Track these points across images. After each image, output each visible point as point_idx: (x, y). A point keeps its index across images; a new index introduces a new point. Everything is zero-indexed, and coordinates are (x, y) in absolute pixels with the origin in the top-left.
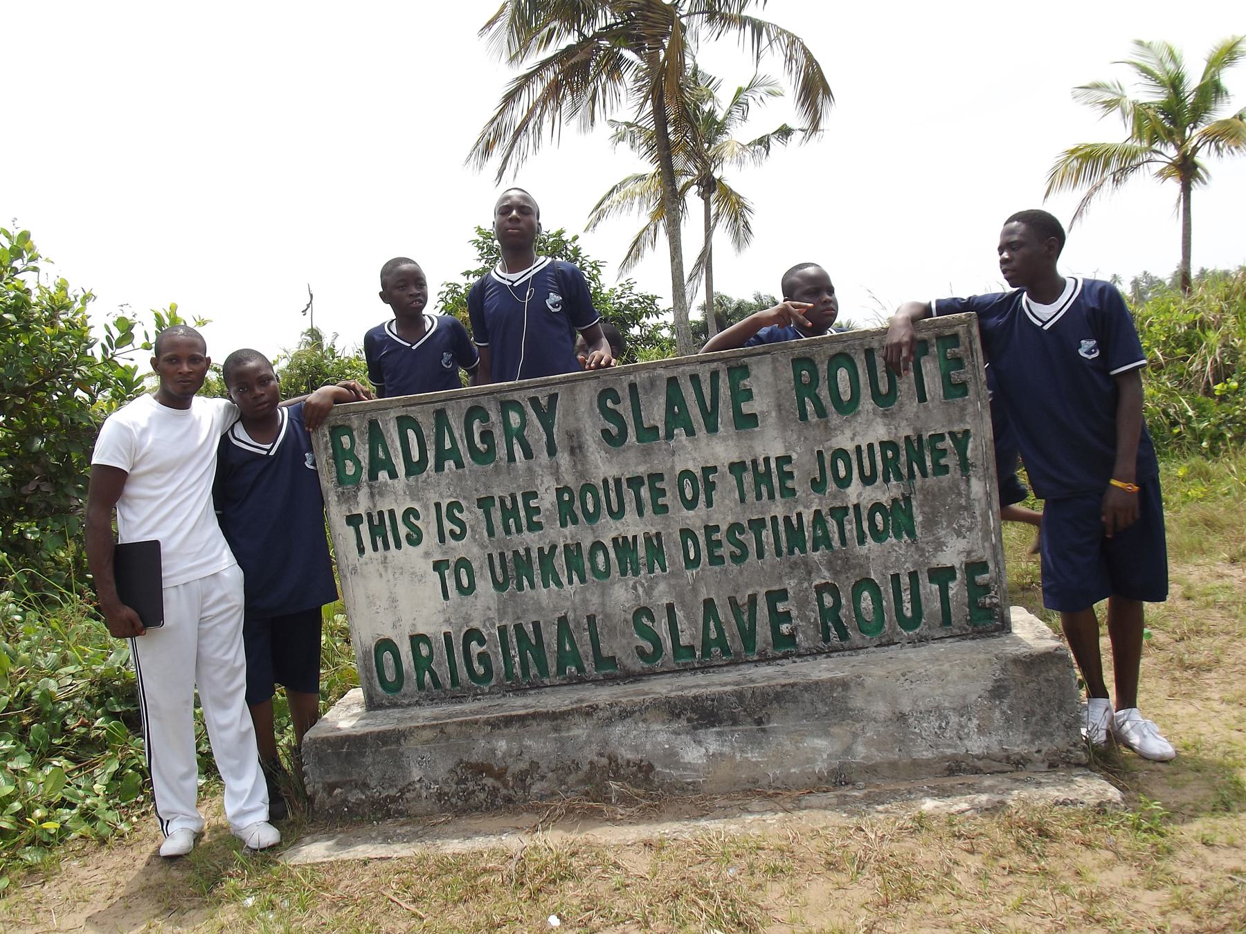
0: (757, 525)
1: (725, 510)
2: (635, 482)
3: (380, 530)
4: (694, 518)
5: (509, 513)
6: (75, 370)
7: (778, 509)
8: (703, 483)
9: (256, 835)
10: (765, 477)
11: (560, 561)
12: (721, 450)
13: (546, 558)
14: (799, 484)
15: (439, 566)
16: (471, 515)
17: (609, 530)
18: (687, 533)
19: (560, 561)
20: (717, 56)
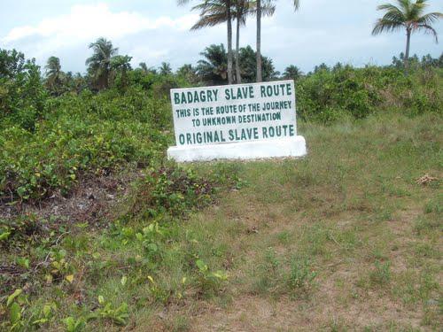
0: (253, 116)
1: (247, 112)
2: (231, 107)
3: (182, 113)
4: (242, 114)
5: (207, 111)
6: (154, 292)
7: (257, 113)
8: (242, 108)
9: (349, 124)
10: (256, 107)
11: (216, 121)
12: (248, 101)
13: (214, 120)
14: (261, 109)
15: (193, 120)
16: (200, 111)
17: (225, 115)
18: (240, 117)
19: (216, 121)
20: (437, 231)
